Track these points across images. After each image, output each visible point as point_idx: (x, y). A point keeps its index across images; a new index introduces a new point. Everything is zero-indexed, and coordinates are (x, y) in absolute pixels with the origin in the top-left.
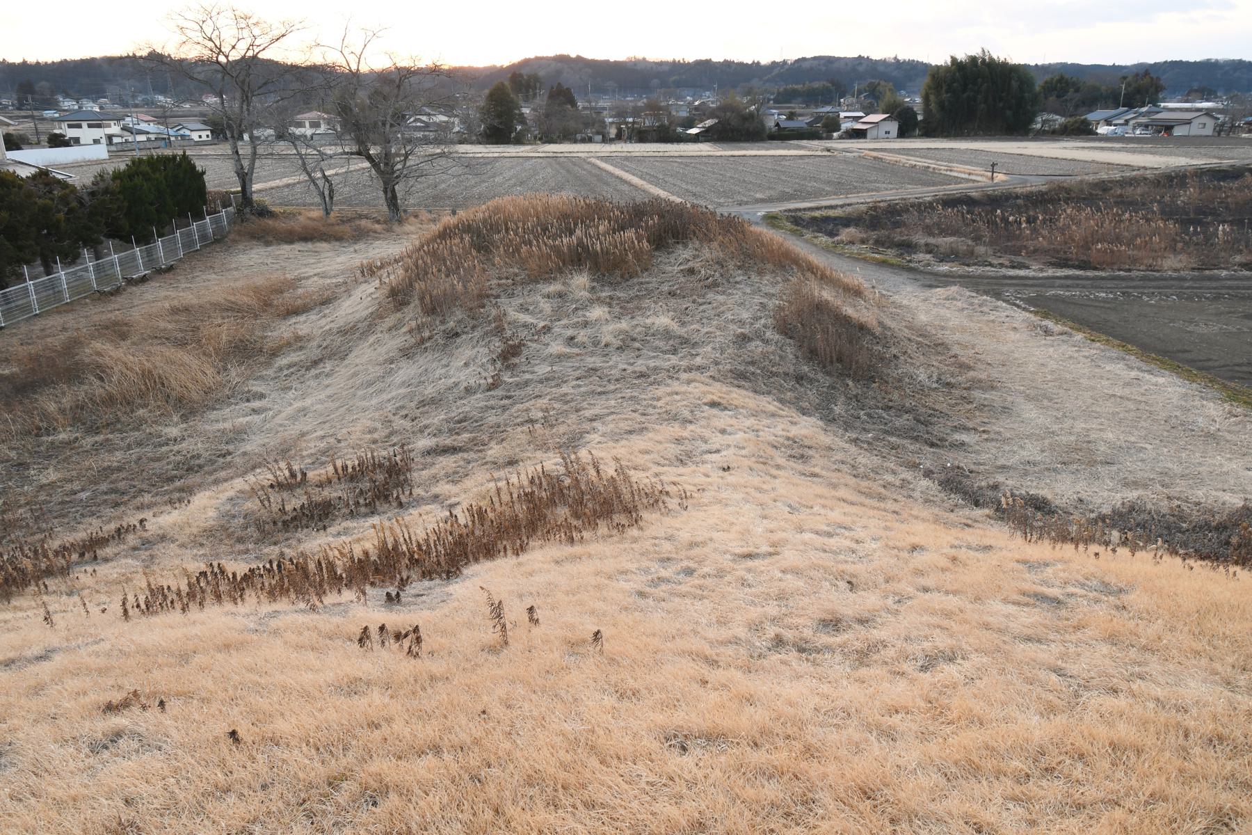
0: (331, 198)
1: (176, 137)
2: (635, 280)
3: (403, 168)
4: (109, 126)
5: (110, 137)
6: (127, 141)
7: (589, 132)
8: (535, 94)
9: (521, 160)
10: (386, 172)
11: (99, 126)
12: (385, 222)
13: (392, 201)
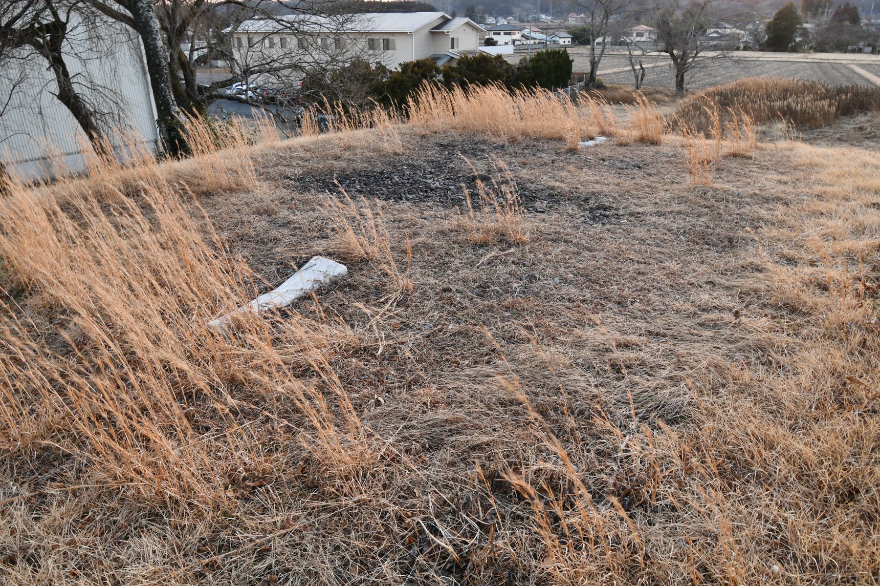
0: (642, 79)
1: (550, 41)
2: (818, 130)
3: (692, 61)
4: (515, 34)
5: (514, 41)
6: (523, 44)
7: (861, 44)
8: (823, 13)
9: (789, 63)
10: (681, 67)
11: (510, 34)
12: (672, 96)
13: (680, 83)
